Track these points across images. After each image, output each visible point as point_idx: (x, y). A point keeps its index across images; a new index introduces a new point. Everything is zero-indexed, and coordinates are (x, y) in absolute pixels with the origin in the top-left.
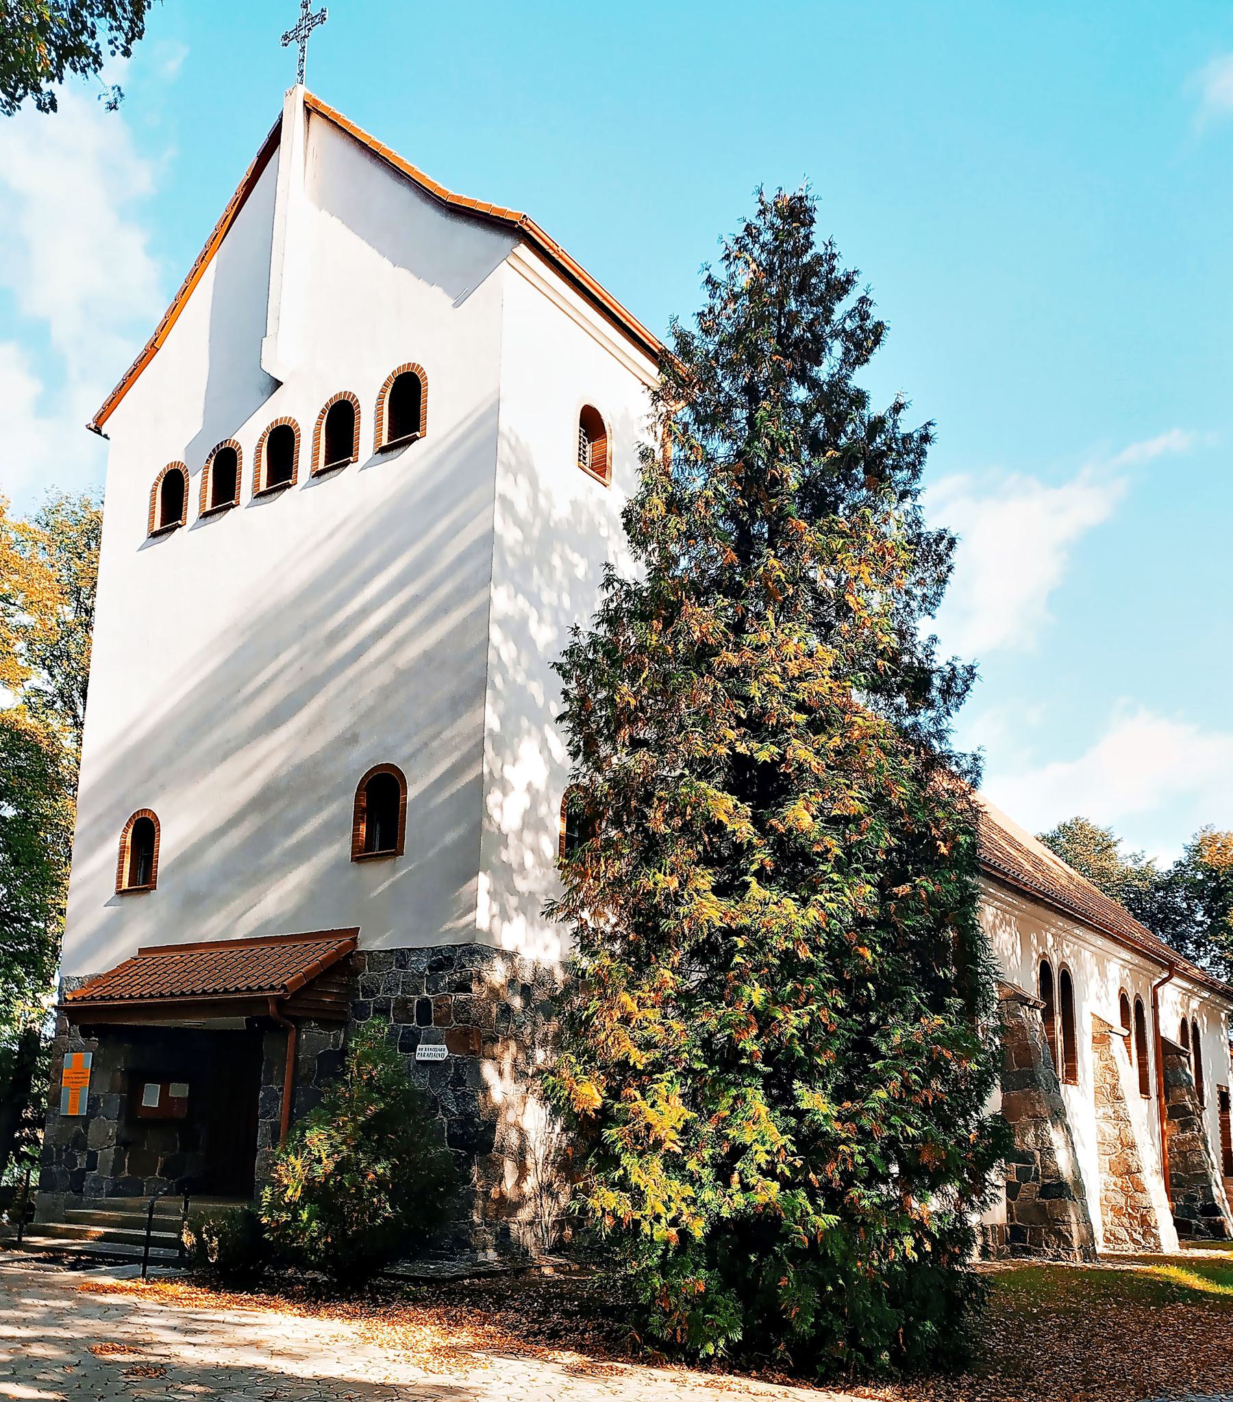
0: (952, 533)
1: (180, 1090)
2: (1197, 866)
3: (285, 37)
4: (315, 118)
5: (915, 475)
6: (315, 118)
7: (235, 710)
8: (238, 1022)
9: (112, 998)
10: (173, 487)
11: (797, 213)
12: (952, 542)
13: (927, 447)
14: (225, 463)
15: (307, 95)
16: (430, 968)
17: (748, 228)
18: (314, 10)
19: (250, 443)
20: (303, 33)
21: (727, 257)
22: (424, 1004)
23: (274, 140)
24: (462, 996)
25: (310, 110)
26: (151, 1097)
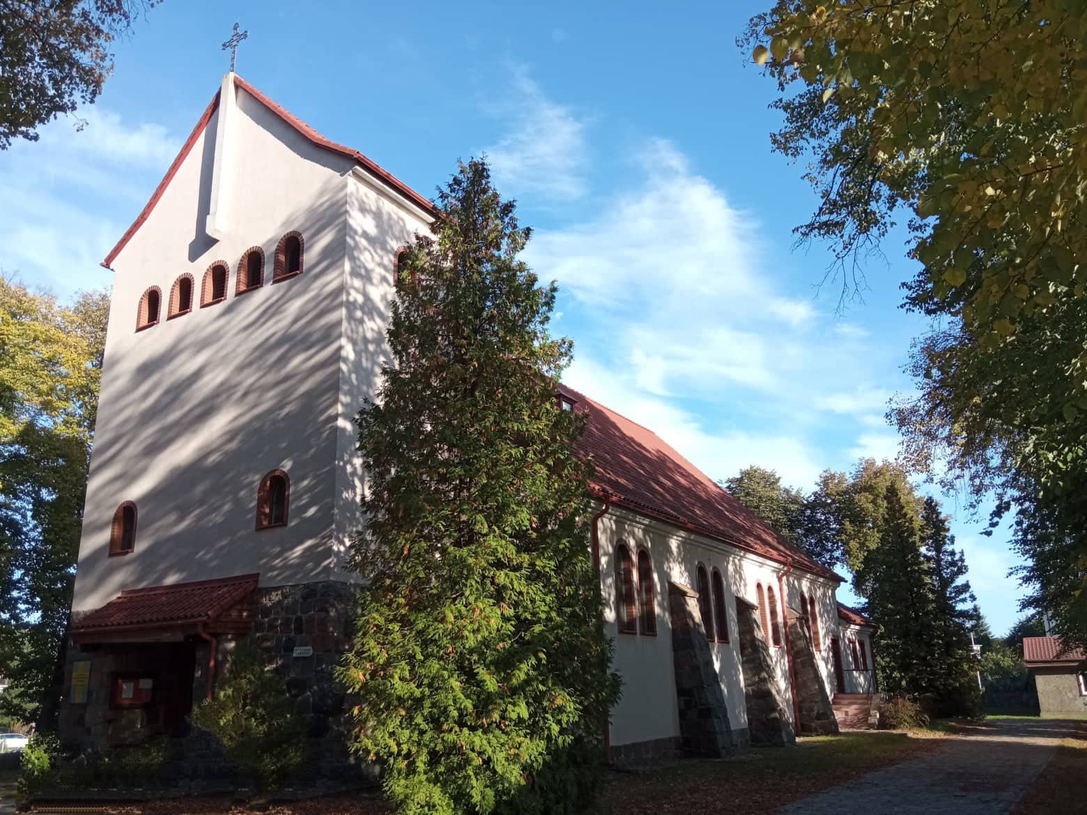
0: (569, 338)
1: (146, 684)
2: (828, 495)
3: (224, 45)
4: (241, 91)
5: (550, 309)
6: (241, 91)
7: (280, 343)
8: (180, 637)
9: (100, 626)
10: (153, 298)
11: (479, 172)
12: (571, 345)
13: (555, 294)
14: (185, 285)
15: (236, 79)
16: (303, 597)
17: (455, 179)
18: (240, 31)
19: (199, 270)
20: (235, 43)
21: (441, 197)
22: (299, 620)
23: (216, 105)
24: (323, 614)
25: (237, 86)
26: (127, 690)
